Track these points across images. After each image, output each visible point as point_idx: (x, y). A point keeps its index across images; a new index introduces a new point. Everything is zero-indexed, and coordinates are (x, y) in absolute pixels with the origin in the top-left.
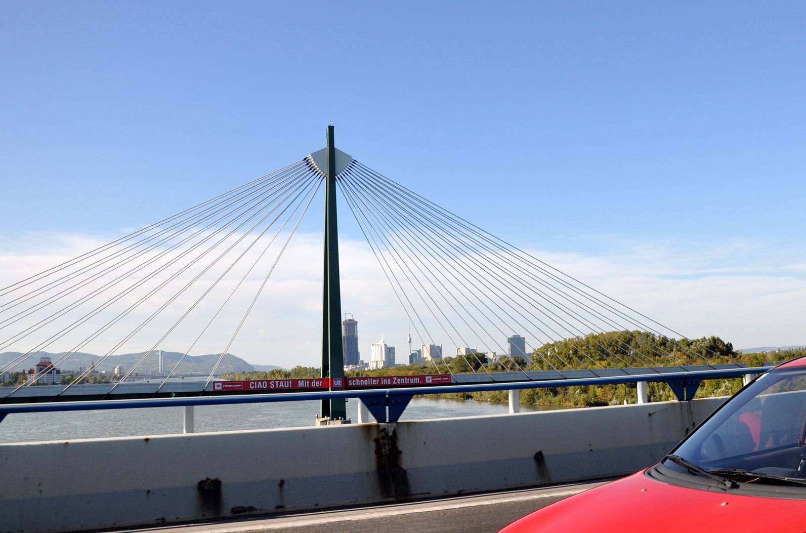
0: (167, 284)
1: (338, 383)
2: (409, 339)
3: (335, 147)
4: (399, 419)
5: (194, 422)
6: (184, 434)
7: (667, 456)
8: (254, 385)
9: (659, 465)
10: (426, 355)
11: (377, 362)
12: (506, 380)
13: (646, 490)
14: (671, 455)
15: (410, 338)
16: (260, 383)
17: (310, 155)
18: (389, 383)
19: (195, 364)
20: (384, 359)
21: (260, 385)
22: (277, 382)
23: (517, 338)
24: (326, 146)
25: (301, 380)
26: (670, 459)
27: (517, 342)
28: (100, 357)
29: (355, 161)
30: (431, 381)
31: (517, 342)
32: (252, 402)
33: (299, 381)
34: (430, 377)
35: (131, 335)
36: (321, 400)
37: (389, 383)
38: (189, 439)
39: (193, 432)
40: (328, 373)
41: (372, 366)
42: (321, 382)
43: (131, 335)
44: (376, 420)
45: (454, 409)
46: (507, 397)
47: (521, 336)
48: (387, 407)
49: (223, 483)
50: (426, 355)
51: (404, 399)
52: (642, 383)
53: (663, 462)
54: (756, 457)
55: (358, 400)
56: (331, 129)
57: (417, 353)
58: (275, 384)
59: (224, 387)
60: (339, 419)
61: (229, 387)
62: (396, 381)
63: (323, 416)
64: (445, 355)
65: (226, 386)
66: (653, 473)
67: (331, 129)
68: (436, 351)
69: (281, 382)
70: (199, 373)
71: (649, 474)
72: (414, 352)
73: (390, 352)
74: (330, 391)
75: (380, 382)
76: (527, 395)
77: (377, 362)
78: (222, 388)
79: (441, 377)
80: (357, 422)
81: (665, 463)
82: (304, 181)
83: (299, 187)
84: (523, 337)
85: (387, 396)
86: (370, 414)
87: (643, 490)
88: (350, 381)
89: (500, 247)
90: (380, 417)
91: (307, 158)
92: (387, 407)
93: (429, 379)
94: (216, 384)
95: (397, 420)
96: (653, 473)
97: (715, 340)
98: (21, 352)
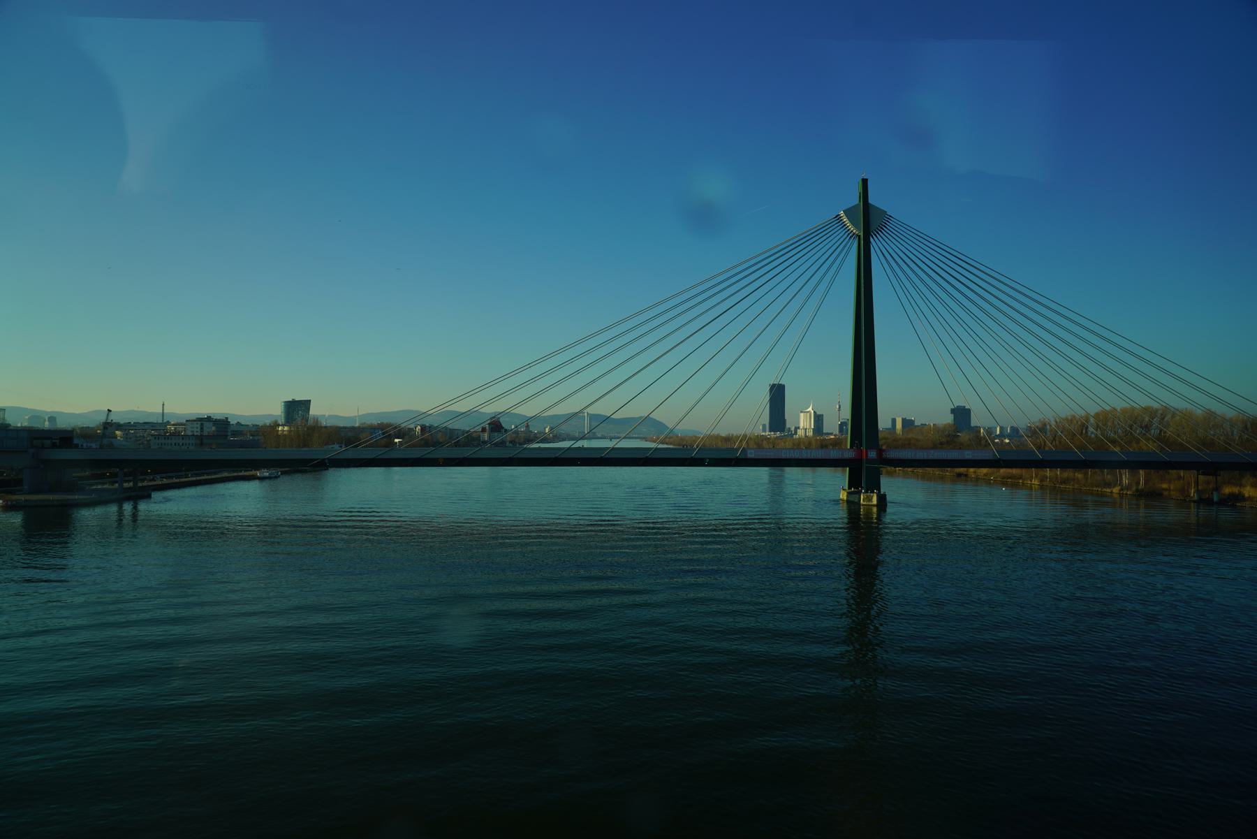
0: (1159, 365)
2: (838, 407)
3: (870, 202)
5: (328, 425)
11: (806, 429)
15: (840, 406)
20: (812, 427)
24: (857, 202)
29: (890, 216)
35: (511, 374)
36: (848, 469)
40: (241, 471)
41: (801, 433)
43: (511, 374)
45: (441, 440)
54: (243, 473)
56: (865, 182)
63: (850, 488)
67: (865, 182)
73: (819, 419)
77: (806, 429)
82: (817, 238)
89: (969, 312)
91: (838, 215)
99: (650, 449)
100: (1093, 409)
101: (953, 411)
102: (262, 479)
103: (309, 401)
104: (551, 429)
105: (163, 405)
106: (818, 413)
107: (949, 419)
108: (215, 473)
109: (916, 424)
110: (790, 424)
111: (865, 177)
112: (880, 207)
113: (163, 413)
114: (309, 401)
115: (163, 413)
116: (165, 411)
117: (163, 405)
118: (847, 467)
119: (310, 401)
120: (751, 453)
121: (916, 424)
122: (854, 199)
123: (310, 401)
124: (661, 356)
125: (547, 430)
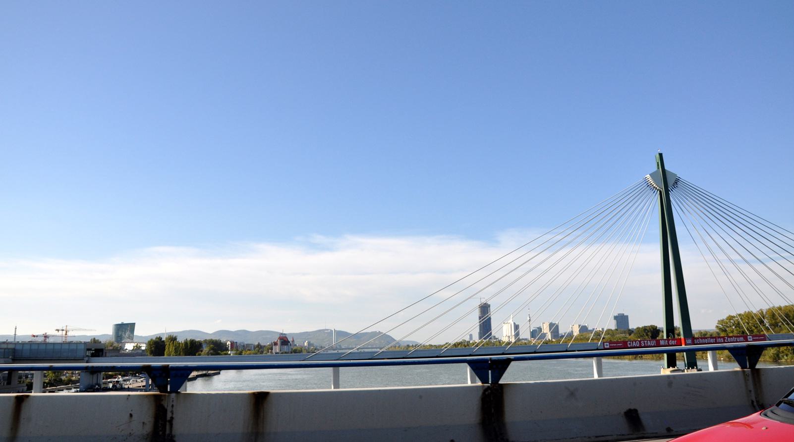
1: (689, 341)
3: (666, 169)
4: (501, 380)
6: (332, 389)
7: (781, 400)
8: (630, 344)
9: (774, 408)
10: (546, 330)
12: (555, 350)
13: (767, 428)
14: (786, 399)
16: (634, 342)
17: (649, 175)
18: (723, 341)
19: (355, 340)
21: (634, 344)
22: (646, 342)
23: (621, 316)
25: (662, 340)
26: (785, 403)
27: (622, 320)
28: (351, 334)
30: (608, 347)
31: (622, 320)
32: (573, 358)
33: (661, 341)
34: (608, 344)
37: (723, 341)
38: (612, 381)
39: (339, 388)
42: (676, 341)
44: (739, 366)
46: (663, 356)
47: (625, 315)
48: (490, 371)
49: (640, 412)
50: (546, 330)
51: (505, 364)
52: (334, 370)
53: (778, 405)
55: (466, 364)
56: (661, 155)
57: (538, 329)
58: (644, 343)
59: (611, 346)
60: (694, 368)
61: (614, 346)
62: (727, 340)
64: (633, 325)
65: (612, 345)
66: (769, 414)
67: (661, 155)
68: (554, 328)
69: (649, 341)
70: (370, 347)
71: (766, 415)
72: (534, 329)
74: (683, 346)
75: (716, 340)
76: (773, 354)
77: (509, 337)
78: (610, 346)
79: (617, 344)
80: (467, 383)
81: (780, 406)
83: (633, 199)
84: (627, 315)
85: (489, 362)
86: (477, 378)
87: (764, 428)
88: (695, 340)
90: (484, 380)
92: (490, 371)
93: (607, 345)
94: (605, 344)
95: (755, 366)
96: (769, 414)
97: (730, 316)
98: (350, 333)
99: (377, 352)
100: (765, 307)
101: (616, 318)
102: (747, 386)
103: (134, 324)
104: (309, 344)
105: (16, 328)
106: (517, 324)
107: (612, 325)
108: (652, 374)
109: (589, 329)
110: (494, 332)
111: (660, 152)
112: (672, 171)
113: (15, 335)
114: (134, 324)
115: (15, 335)
116: (17, 333)
117: (16, 328)
118: (675, 355)
119: (135, 324)
120: (607, 345)
121: (589, 329)
122: (654, 167)
123: (135, 324)
124: (752, 230)
125: (306, 344)
